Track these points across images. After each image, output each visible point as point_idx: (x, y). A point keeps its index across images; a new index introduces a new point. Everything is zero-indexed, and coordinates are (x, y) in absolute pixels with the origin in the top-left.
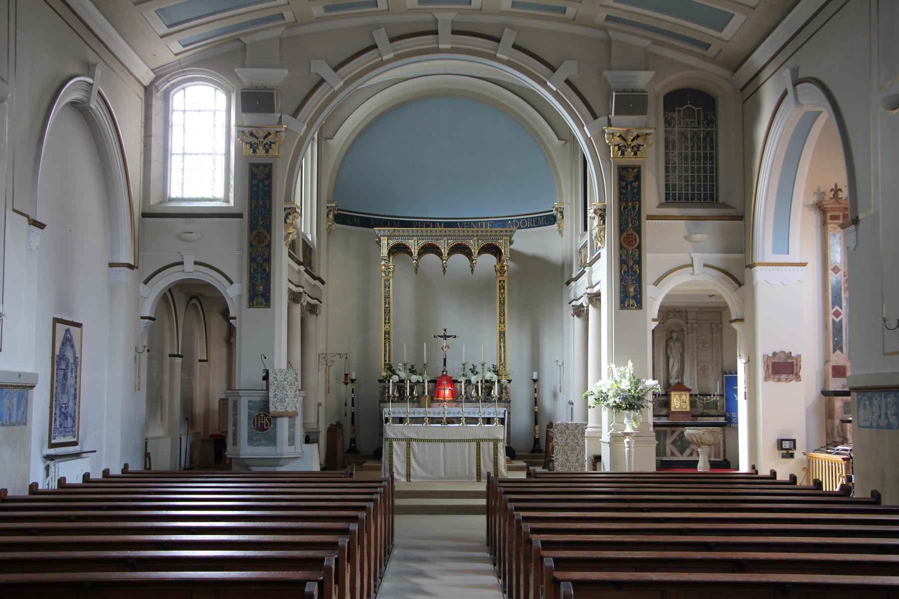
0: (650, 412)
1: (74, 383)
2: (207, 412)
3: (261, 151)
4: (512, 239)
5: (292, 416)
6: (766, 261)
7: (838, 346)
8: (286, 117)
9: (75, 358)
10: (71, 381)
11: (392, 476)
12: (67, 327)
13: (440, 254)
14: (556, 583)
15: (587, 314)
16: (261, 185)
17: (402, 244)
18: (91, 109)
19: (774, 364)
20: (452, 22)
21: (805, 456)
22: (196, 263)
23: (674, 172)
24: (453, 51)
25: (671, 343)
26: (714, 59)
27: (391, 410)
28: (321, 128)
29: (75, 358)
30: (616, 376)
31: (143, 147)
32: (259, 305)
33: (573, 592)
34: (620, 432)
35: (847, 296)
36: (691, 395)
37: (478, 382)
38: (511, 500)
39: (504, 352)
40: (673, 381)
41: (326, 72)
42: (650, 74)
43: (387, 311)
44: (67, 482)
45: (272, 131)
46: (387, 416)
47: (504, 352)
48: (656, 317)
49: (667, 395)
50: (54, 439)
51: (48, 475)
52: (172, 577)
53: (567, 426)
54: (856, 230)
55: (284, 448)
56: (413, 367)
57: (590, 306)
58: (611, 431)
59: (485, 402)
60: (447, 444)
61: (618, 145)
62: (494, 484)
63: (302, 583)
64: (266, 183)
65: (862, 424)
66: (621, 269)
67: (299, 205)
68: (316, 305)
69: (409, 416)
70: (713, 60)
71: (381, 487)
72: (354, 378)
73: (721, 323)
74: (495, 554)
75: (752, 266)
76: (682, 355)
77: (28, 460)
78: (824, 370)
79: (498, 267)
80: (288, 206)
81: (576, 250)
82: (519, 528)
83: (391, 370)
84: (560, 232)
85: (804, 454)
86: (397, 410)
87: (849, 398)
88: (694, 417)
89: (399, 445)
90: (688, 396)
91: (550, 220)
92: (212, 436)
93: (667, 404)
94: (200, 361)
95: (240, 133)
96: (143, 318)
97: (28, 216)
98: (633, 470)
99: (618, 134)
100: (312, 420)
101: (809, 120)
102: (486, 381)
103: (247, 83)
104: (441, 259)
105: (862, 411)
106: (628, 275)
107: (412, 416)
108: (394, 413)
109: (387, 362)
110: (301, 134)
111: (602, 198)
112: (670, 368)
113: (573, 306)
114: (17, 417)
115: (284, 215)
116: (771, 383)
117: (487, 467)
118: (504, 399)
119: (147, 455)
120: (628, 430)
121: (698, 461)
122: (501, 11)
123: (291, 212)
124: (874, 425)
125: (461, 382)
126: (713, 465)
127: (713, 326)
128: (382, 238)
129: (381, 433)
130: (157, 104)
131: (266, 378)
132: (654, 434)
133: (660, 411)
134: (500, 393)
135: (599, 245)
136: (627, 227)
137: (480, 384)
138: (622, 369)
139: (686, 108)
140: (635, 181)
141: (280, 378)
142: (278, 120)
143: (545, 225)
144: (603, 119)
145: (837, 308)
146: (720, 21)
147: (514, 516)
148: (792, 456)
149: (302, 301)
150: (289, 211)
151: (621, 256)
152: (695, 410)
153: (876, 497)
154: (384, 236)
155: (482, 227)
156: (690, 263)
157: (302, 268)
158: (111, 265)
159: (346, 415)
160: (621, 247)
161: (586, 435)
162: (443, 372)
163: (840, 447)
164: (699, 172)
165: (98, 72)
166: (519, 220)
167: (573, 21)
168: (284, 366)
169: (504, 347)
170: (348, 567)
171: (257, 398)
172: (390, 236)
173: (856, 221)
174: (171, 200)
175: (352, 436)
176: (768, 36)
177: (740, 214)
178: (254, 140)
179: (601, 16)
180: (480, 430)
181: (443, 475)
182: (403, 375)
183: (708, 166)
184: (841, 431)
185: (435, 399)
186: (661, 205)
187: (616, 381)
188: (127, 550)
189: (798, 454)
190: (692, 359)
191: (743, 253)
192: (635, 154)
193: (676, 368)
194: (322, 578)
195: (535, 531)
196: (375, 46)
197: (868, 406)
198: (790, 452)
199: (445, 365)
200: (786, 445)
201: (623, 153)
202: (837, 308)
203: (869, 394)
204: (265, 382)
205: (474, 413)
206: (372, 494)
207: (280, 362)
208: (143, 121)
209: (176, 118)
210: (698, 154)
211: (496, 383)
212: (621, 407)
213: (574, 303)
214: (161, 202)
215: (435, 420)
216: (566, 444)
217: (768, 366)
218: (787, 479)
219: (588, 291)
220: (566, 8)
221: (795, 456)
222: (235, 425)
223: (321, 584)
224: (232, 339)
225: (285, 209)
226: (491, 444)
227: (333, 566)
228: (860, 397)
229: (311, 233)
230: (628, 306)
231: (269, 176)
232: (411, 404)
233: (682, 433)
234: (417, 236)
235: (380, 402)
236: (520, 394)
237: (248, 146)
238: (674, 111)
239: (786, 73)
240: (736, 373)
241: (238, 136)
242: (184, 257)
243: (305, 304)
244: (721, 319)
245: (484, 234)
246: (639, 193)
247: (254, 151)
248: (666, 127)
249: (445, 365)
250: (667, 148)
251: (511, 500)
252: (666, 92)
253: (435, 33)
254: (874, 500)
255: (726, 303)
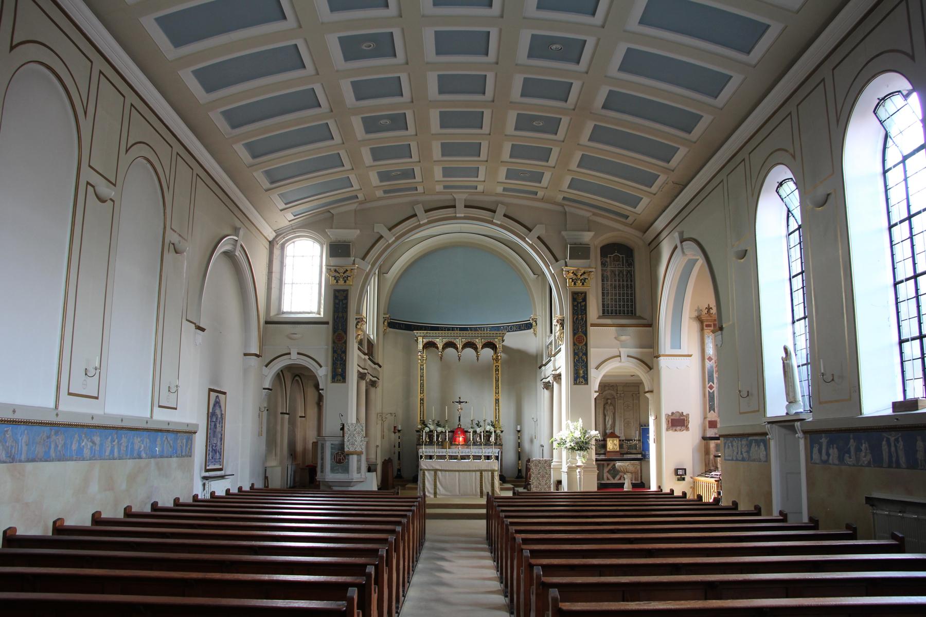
0: (593, 452)
1: (221, 430)
2: (305, 451)
3: (341, 282)
4: (504, 338)
5: (359, 454)
6: (667, 353)
7: (712, 408)
8: (358, 260)
9: (222, 414)
10: (219, 429)
11: (424, 494)
12: (217, 394)
13: (457, 348)
14: (531, 566)
15: (553, 388)
16: (341, 303)
17: (432, 342)
18: (236, 256)
19: (672, 420)
20: (465, 200)
21: (692, 480)
22: (299, 354)
23: (608, 296)
24: (465, 218)
25: (607, 407)
26: (631, 224)
27: (424, 450)
28: (380, 267)
29: (222, 414)
30: (572, 427)
31: (267, 279)
32: (339, 381)
33: (542, 573)
34: (574, 465)
35: (717, 376)
36: (620, 440)
37: (481, 432)
38: (503, 511)
39: (499, 412)
40: (608, 431)
41: (384, 231)
42: (591, 234)
43: (422, 385)
44: (216, 494)
45: (349, 268)
46: (421, 454)
47: (499, 412)
48: (597, 390)
49: (605, 440)
50: (208, 466)
51: (204, 489)
52: (280, 560)
53: (539, 461)
54: (722, 334)
55: (354, 475)
56: (438, 422)
57: (555, 382)
58: (568, 465)
59: (486, 445)
60: (461, 473)
61: (572, 278)
62: (492, 502)
63: (364, 566)
64: (344, 302)
65: (727, 458)
66: (574, 358)
67: (365, 316)
68: (375, 381)
69: (436, 454)
70: (631, 225)
71: (417, 502)
72: (400, 429)
73: (639, 393)
74: (492, 546)
75: (658, 357)
76: (614, 414)
77: (192, 479)
78: (704, 423)
79: (494, 357)
80: (358, 317)
81: (545, 346)
82: (507, 530)
83: (424, 424)
84: (535, 334)
85: (691, 478)
86: (428, 450)
87: (719, 441)
88: (622, 455)
89: (429, 473)
90: (618, 441)
91: (528, 326)
92: (307, 466)
93: (604, 446)
94: (300, 417)
95: (329, 270)
96: (264, 389)
97: (195, 324)
98: (582, 490)
99: (572, 272)
100: (372, 456)
101: (691, 264)
102: (487, 432)
103: (333, 238)
104: (458, 351)
105: (727, 450)
106: (579, 363)
107: (438, 454)
108: (426, 452)
109: (422, 419)
110: (367, 271)
111: (562, 313)
112: (606, 423)
113: (544, 382)
114: (186, 453)
115: (355, 322)
116: (671, 432)
117: (487, 488)
118: (498, 444)
119: (266, 478)
120: (579, 463)
121: (624, 483)
122: (496, 194)
123: (360, 320)
124: (734, 459)
125: (470, 432)
126: (634, 486)
127: (634, 395)
128: (419, 338)
129: (418, 466)
130: (277, 252)
131: (342, 429)
132: (596, 466)
133: (599, 451)
134: (496, 439)
135: (560, 343)
136: (579, 331)
137: (482, 434)
138: (575, 424)
139: (615, 255)
140: (583, 302)
141: (352, 429)
142: (352, 261)
143: (525, 330)
144: (562, 262)
145: (711, 383)
146: (635, 202)
147: (504, 522)
148: (684, 479)
149: (367, 378)
150: (358, 320)
151: (574, 350)
152: (623, 450)
153: (735, 505)
154: (420, 336)
155: (484, 331)
156: (619, 354)
157: (367, 357)
158: (245, 355)
159: (394, 453)
160: (574, 344)
161: (552, 467)
162: (458, 425)
163: (713, 473)
164: (623, 296)
165: (241, 232)
166: (508, 326)
167: (542, 200)
168: (354, 421)
169: (498, 409)
170: (395, 555)
171: (337, 441)
172: (424, 336)
173: (721, 329)
174: (284, 313)
175: (398, 467)
176: (664, 211)
177: (650, 323)
178: (337, 275)
179: (560, 197)
180: (482, 464)
181: (458, 494)
182: (432, 427)
183: (629, 292)
184: (714, 463)
185: (453, 443)
186: (599, 317)
187: (571, 432)
188: (252, 541)
189: (687, 478)
190: (621, 417)
191: (651, 348)
192: (583, 284)
193: (610, 423)
194: (377, 563)
195: (518, 532)
196: (415, 215)
197: (731, 447)
198: (683, 477)
199: (459, 421)
200: (680, 472)
201: (575, 284)
202: (711, 383)
203: (731, 439)
204: (342, 431)
205: (479, 453)
206: (411, 506)
207: (352, 418)
208: (268, 263)
209: (288, 261)
210: (623, 285)
211: (493, 433)
212: (574, 449)
213: (544, 380)
214: (278, 314)
215: (453, 457)
216: (539, 473)
217: (668, 422)
218: (681, 494)
219: (553, 373)
220: (537, 192)
221: (686, 479)
222: (322, 459)
223: (376, 567)
224: (321, 403)
225: (356, 319)
226: (490, 473)
227: (385, 555)
228: (725, 441)
229: (373, 334)
230: (579, 382)
231: (346, 297)
232: (437, 446)
233: (614, 465)
234: (442, 336)
235: (417, 445)
236: (509, 440)
237: (333, 278)
238: (607, 257)
239: (676, 235)
240: (648, 426)
241: (327, 272)
242: (292, 349)
243: (368, 380)
244: (639, 391)
245: (485, 335)
246: (585, 309)
247: (337, 282)
248: (602, 267)
249: (459, 421)
250: (603, 280)
251: (503, 511)
252: (601, 245)
253: (454, 207)
254: (733, 507)
255: (642, 380)
